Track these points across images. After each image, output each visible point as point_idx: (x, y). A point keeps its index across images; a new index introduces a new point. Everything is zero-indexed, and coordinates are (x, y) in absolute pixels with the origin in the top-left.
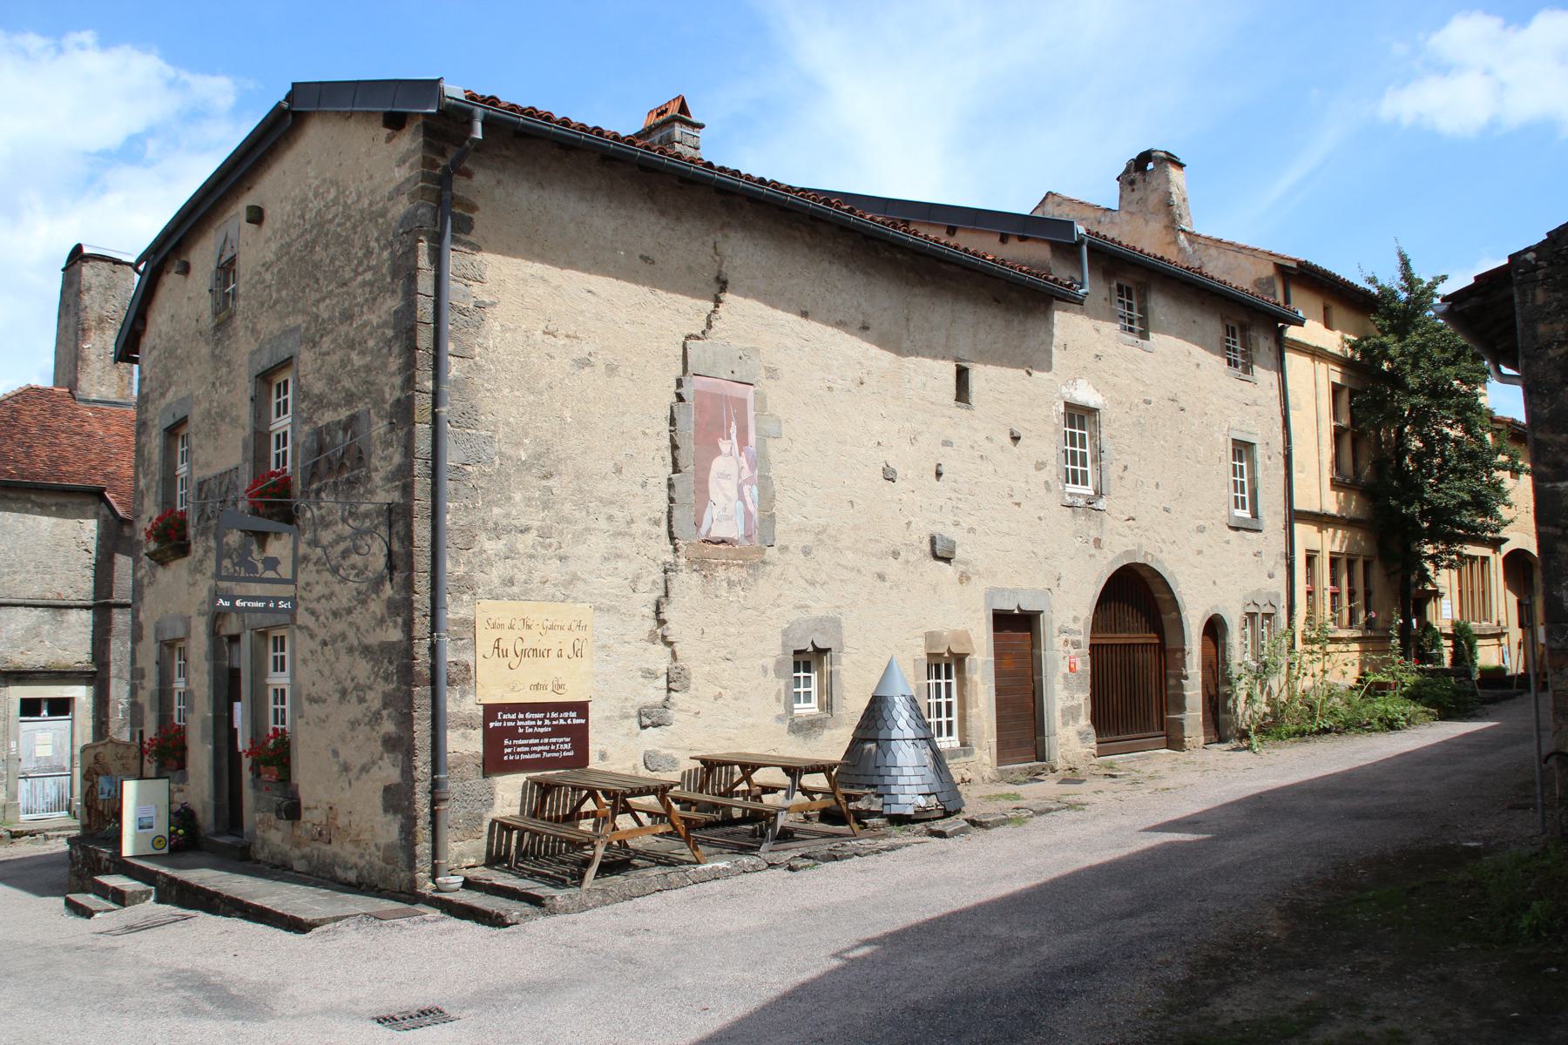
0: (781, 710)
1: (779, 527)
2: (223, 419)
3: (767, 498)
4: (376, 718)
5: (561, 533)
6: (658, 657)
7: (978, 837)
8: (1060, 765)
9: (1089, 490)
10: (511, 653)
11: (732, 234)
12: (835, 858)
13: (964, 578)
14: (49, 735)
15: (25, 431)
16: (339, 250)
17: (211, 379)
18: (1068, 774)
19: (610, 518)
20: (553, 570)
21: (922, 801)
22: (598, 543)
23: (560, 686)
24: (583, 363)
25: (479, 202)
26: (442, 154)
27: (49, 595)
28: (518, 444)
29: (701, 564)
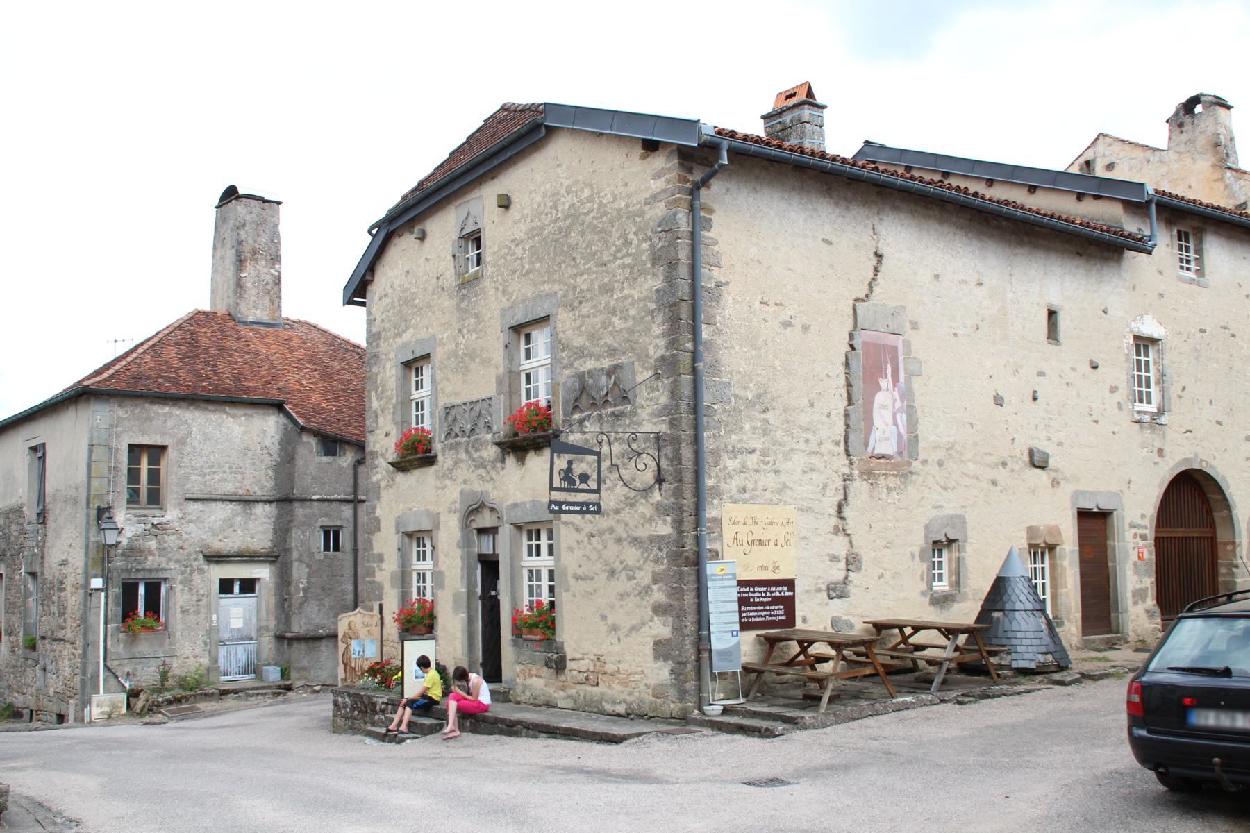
0: (924, 587)
1: (921, 445)
2: (473, 359)
3: (912, 423)
4: (647, 590)
5: (775, 453)
6: (839, 546)
7: (1090, 688)
8: (1132, 637)
9: (1153, 408)
10: (745, 543)
11: (885, 218)
12: (989, 697)
13: (1055, 483)
14: (241, 610)
15: (207, 352)
16: (596, 238)
17: (458, 326)
18: (1139, 645)
19: (807, 441)
20: (769, 480)
21: (1041, 658)
22: (799, 460)
23: (777, 568)
24: (787, 325)
25: (715, 206)
26: (690, 171)
27: (240, 492)
28: (746, 387)
29: (868, 475)
